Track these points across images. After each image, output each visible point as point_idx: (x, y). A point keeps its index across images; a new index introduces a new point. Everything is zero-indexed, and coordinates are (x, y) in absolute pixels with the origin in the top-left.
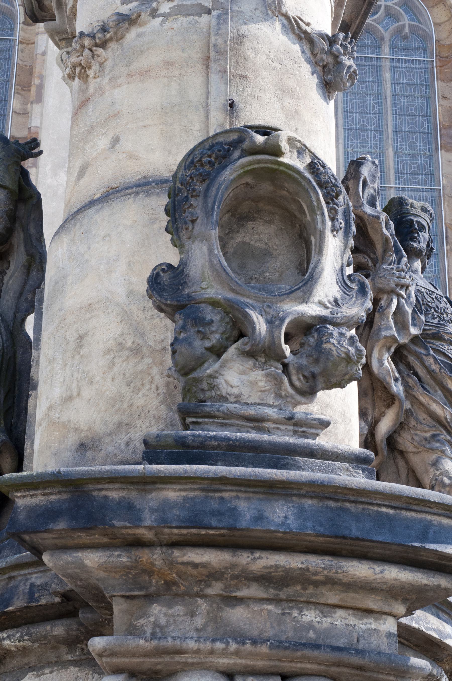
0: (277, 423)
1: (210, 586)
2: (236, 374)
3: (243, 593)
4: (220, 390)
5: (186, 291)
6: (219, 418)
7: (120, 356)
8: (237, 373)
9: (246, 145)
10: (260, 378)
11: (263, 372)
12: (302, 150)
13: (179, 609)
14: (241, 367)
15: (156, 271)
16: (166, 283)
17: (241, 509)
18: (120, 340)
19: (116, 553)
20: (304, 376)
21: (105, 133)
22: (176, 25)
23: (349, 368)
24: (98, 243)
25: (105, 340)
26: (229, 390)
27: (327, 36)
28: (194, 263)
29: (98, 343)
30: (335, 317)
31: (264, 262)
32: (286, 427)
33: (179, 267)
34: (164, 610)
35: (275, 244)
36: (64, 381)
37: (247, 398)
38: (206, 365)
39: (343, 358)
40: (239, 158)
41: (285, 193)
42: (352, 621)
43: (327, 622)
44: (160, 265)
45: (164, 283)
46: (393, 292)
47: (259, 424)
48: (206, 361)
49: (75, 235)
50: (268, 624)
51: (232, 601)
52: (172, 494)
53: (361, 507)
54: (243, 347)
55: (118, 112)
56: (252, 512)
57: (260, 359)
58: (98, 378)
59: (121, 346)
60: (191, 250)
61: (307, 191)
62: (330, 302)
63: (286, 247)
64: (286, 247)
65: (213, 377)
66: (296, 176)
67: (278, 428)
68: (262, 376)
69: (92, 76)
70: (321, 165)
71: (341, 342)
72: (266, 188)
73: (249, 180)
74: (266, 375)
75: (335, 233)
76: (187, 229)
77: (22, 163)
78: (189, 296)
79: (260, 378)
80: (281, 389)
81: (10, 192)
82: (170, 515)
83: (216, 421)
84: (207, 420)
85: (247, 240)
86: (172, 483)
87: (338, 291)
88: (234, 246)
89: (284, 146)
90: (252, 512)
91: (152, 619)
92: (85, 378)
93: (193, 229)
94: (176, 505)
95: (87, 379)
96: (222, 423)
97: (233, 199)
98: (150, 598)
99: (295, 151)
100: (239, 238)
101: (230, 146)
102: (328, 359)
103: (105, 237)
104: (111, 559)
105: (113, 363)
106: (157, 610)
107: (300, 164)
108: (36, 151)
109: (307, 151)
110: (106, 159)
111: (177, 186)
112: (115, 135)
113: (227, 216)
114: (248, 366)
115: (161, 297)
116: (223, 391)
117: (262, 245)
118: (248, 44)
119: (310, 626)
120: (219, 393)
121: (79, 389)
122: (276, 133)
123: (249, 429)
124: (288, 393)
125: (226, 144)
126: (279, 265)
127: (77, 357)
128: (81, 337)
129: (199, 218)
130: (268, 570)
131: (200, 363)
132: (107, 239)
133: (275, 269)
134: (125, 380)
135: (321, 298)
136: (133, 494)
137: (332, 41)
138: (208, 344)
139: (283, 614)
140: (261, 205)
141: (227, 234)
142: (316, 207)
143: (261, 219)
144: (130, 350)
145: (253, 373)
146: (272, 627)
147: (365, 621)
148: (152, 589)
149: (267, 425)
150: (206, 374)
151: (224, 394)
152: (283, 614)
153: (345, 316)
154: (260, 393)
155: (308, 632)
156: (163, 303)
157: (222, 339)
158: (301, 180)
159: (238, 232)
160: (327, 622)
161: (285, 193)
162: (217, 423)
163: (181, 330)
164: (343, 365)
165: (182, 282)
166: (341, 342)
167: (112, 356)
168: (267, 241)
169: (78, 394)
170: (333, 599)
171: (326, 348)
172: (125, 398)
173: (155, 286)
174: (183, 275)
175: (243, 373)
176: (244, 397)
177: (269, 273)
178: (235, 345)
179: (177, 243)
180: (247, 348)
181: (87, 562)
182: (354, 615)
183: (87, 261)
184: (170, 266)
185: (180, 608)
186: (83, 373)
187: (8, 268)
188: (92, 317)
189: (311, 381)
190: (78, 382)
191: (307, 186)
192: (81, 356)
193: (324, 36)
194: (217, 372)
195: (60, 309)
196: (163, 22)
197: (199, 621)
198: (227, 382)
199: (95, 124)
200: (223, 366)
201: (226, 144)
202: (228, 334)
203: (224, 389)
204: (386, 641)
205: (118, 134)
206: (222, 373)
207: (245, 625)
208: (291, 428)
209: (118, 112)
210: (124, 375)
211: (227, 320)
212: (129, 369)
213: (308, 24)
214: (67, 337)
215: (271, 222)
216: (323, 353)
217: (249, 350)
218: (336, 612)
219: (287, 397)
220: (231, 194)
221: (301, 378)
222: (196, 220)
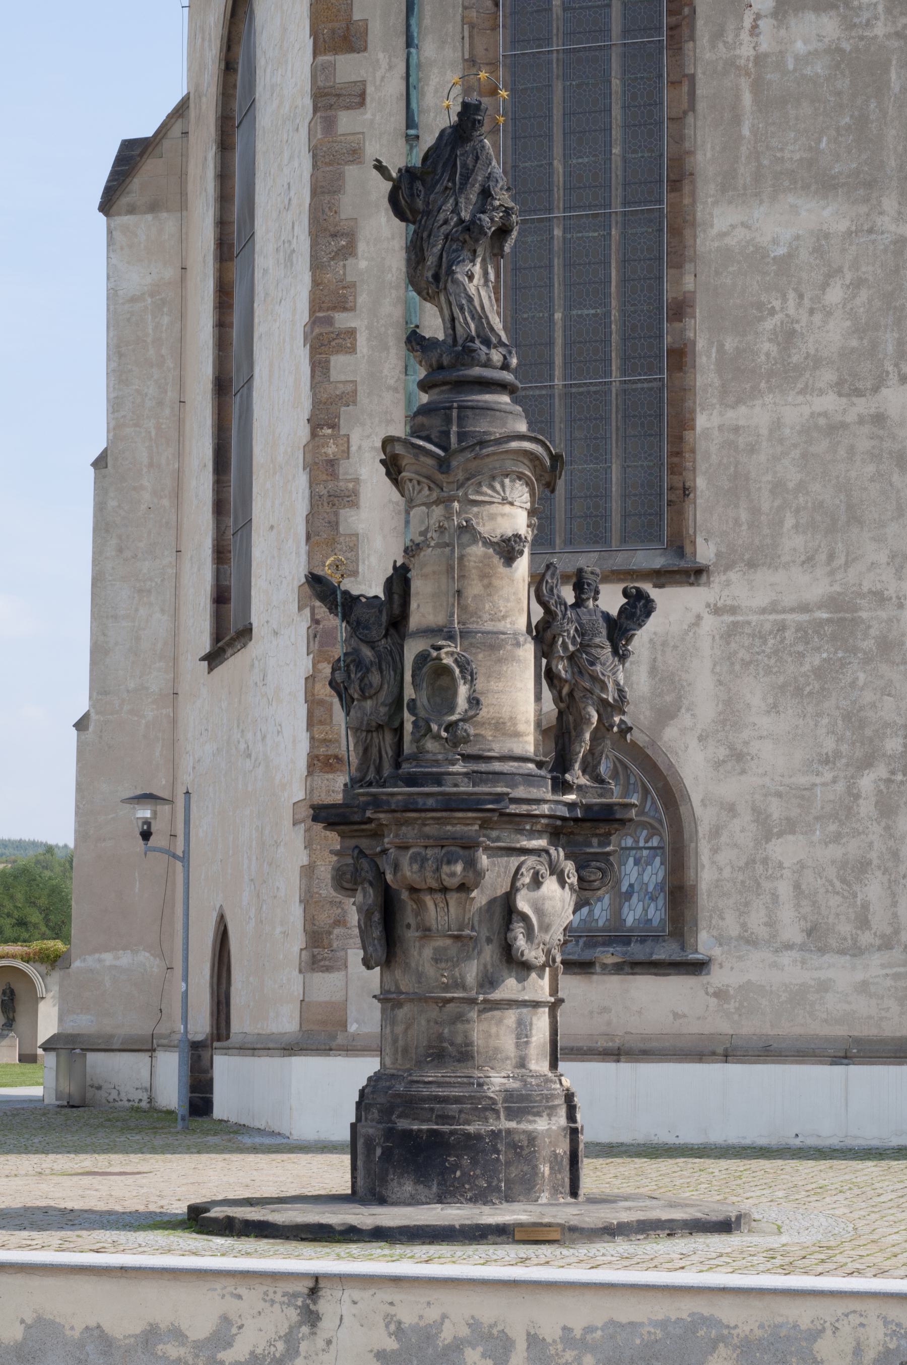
3: (428, 822)
13: (410, 828)
42: (463, 828)
46: (560, 635)
51: (425, 825)
52: (400, 798)
98: (402, 825)
106: (404, 828)
118: (465, 559)
136: (389, 797)
170: (456, 822)
197: (416, 832)
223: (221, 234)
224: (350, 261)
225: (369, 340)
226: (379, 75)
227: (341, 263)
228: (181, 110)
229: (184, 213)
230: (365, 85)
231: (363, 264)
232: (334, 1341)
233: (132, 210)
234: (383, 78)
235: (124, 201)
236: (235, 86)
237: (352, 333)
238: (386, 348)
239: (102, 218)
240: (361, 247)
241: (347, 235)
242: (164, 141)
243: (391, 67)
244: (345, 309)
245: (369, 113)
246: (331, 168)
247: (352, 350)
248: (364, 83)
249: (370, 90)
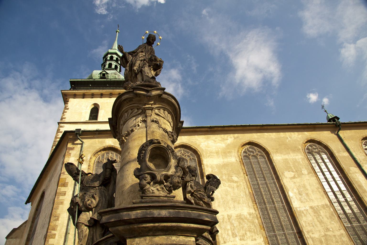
1: (149, 233)
10: (159, 188)
12: (165, 143)
17: (155, 213)
18: (131, 190)
19: (126, 226)
22: (140, 130)
27: (171, 132)
34: (139, 240)
43: (178, 239)
50: (164, 241)
53: (183, 211)
56: (157, 213)
58: (126, 199)
59: (131, 191)
62: (173, 172)
77: (113, 164)
79: (159, 188)
81: (110, 169)
82: (138, 216)
86: (138, 208)
90: (157, 213)
91: (136, 242)
94: (139, 213)
99: (163, 143)
104: (125, 228)
105: (129, 195)
108: (116, 162)
119: (174, 240)
121: (122, 202)
130: (163, 227)
137: (172, 133)
138: (147, 182)
139: (167, 238)
144: (133, 192)
146: (165, 241)
147: (187, 238)
148: (135, 235)
152: (167, 238)
155: (174, 242)
159: (153, 161)
160: (178, 239)
180: (155, 181)
181: (119, 229)
182: (185, 237)
185: (143, 239)
187: (110, 185)
193: (170, 132)
194: (149, 188)
195: (119, 187)
196: (138, 130)
197: (147, 241)
204: (193, 243)
207: (158, 241)
213: (167, 130)
218: (180, 237)
223: (28, 236)
224: (57, 221)
225: (58, 236)
226: (69, 191)
227: (55, 222)
228: (26, 222)
229: (21, 239)
230: (66, 192)
231: (60, 222)
232: (144, 158)
233: (12, 238)
234: (69, 191)
235: (11, 237)
236: (37, 213)
237: (55, 234)
238: (62, 238)
239: (6, 239)
240: (60, 219)
241: (58, 217)
242: (21, 227)
243: (71, 190)
244: (54, 230)
245: (65, 197)
246: (57, 205)
247: (54, 238)
248: (66, 192)
249: (67, 193)
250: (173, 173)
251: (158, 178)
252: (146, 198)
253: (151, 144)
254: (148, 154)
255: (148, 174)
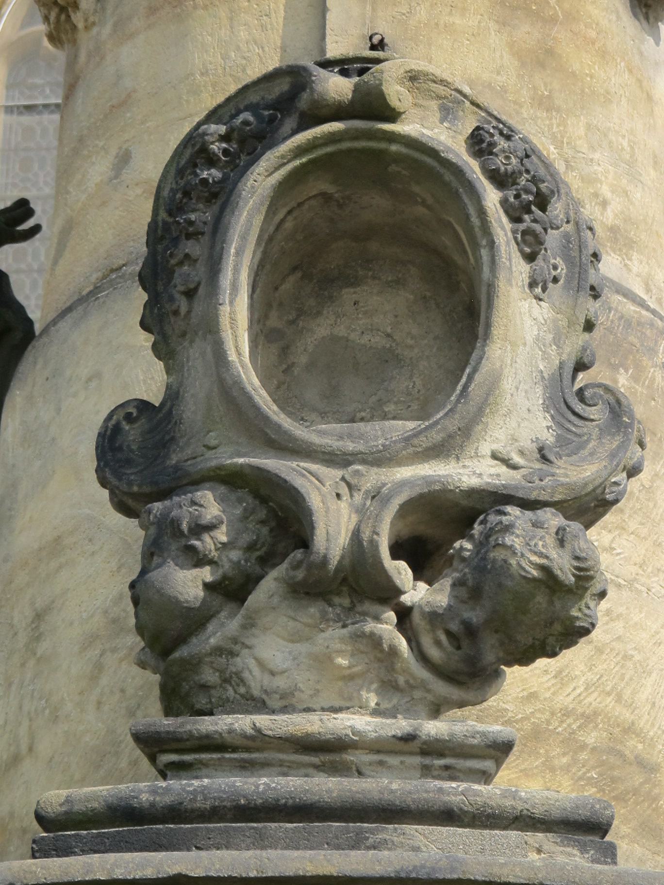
0: (378, 752)
2: (281, 641)
4: (245, 684)
5: (174, 459)
6: (235, 749)
7: (114, 650)
8: (284, 639)
9: (304, 101)
11: (344, 631)
14: (291, 624)
15: (113, 422)
16: (134, 447)
20: (449, 633)
21: (103, 148)
23: (558, 604)
24: (75, 395)
25: (85, 615)
26: (266, 680)
28: (192, 392)
29: (71, 624)
30: (534, 489)
31: (383, 381)
32: (402, 758)
33: (163, 404)
35: (409, 333)
36: (6, 723)
37: (311, 696)
38: (210, 628)
39: (534, 580)
40: (295, 132)
41: (421, 210)
44: (122, 406)
45: (129, 446)
47: (335, 757)
48: (212, 616)
49: (33, 386)
54: (292, 573)
55: (129, 96)
57: (337, 600)
60: (188, 361)
61: (457, 196)
62: (521, 453)
63: (436, 338)
64: (436, 338)
65: (226, 652)
66: (429, 160)
67: (381, 763)
68: (342, 640)
69: (80, 25)
70: (501, 133)
71: (532, 543)
72: (374, 205)
73: (322, 185)
74: (351, 637)
75: (538, 290)
76: (176, 313)
78: (176, 468)
79: (338, 646)
80: (393, 670)
83: (227, 756)
84: (204, 756)
85: (341, 331)
87: (548, 428)
88: (310, 348)
89: (396, 93)
92: (44, 709)
93: (189, 312)
95: (47, 711)
96: (243, 760)
97: (300, 237)
99: (434, 105)
100: (322, 328)
101: (275, 109)
102: (500, 585)
103: (89, 380)
105: (99, 668)
107: (450, 139)
109: (467, 104)
110: (104, 204)
111: (160, 218)
112: (120, 148)
113: (292, 279)
114: (305, 620)
115: (120, 480)
116: (253, 684)
117: (378, 339)
120: (242, 690)
121: (32, 737)
122: (378, 67)
123: (311, 771)
124: (415, 678)
125: (267, 107)
126: (419, 382)
127: (32, 663)
128: (39, 616)
129: (203, 284)
131: (195, 620)
132: (93, 384)
133: (409, 394)
134: (124, 705)
135: (495, 447)
140: (374, 246)
141: (292, 322)
142: (477, 229)
143: (374, 278)
145: (323, 635)
149: (350, 757)
150: (208, 648)
151: (256, 693)
153: (562, 485)
154: (340, 683)
156: (125, 493)
157: (246, 561)
158: (442, 171)
159: (319, 313)
161: (421, 210)
162: (230, 759)
163: (153, 550)
164: (541, 599)
165: (167, 437)
166: (532, 543)
167: (97, 652)
168: (389, 330)
169: (31, 749)
171: (494, 561)
172: (123, 745)
173: (109, 456)
174: (170, 422)
175: (295, 638)
176: (304, 696)
177: (396, 403)
178: (274, 574)
179: (164, 350)
180: (300, 575)
183: (54, 439)
184: (143, 406)
186: (41, 699)
188: (60, 567)
189: (465, 643)
190: (31, 720)
191: (455, 183)
192: (39, 660)
194: (235, 641)
198: (260, 663)
199: (85, 132)
200: (249, 625)
201: (267, 107)
202: (264, 549)
203: (256, 681)
205: (125, 147)
206: (247, 642)
208: (417, 760)
209: (129, 96)
210: (123, 691)
211: (262, 514)
212: (133, 678)
214: (15, 621)
215: (399, 283)
216: (489, 572)
217: (305, 580)
219: (412, 687)
220: (289, 225)
221: (443, 638)
222: (196, 289)
232: (201, 291)
250: (517, 459)
251: (336, 522)
252: (188, 758)
253: (290, 123)
254: (239, 253)
255: (232, 480)
